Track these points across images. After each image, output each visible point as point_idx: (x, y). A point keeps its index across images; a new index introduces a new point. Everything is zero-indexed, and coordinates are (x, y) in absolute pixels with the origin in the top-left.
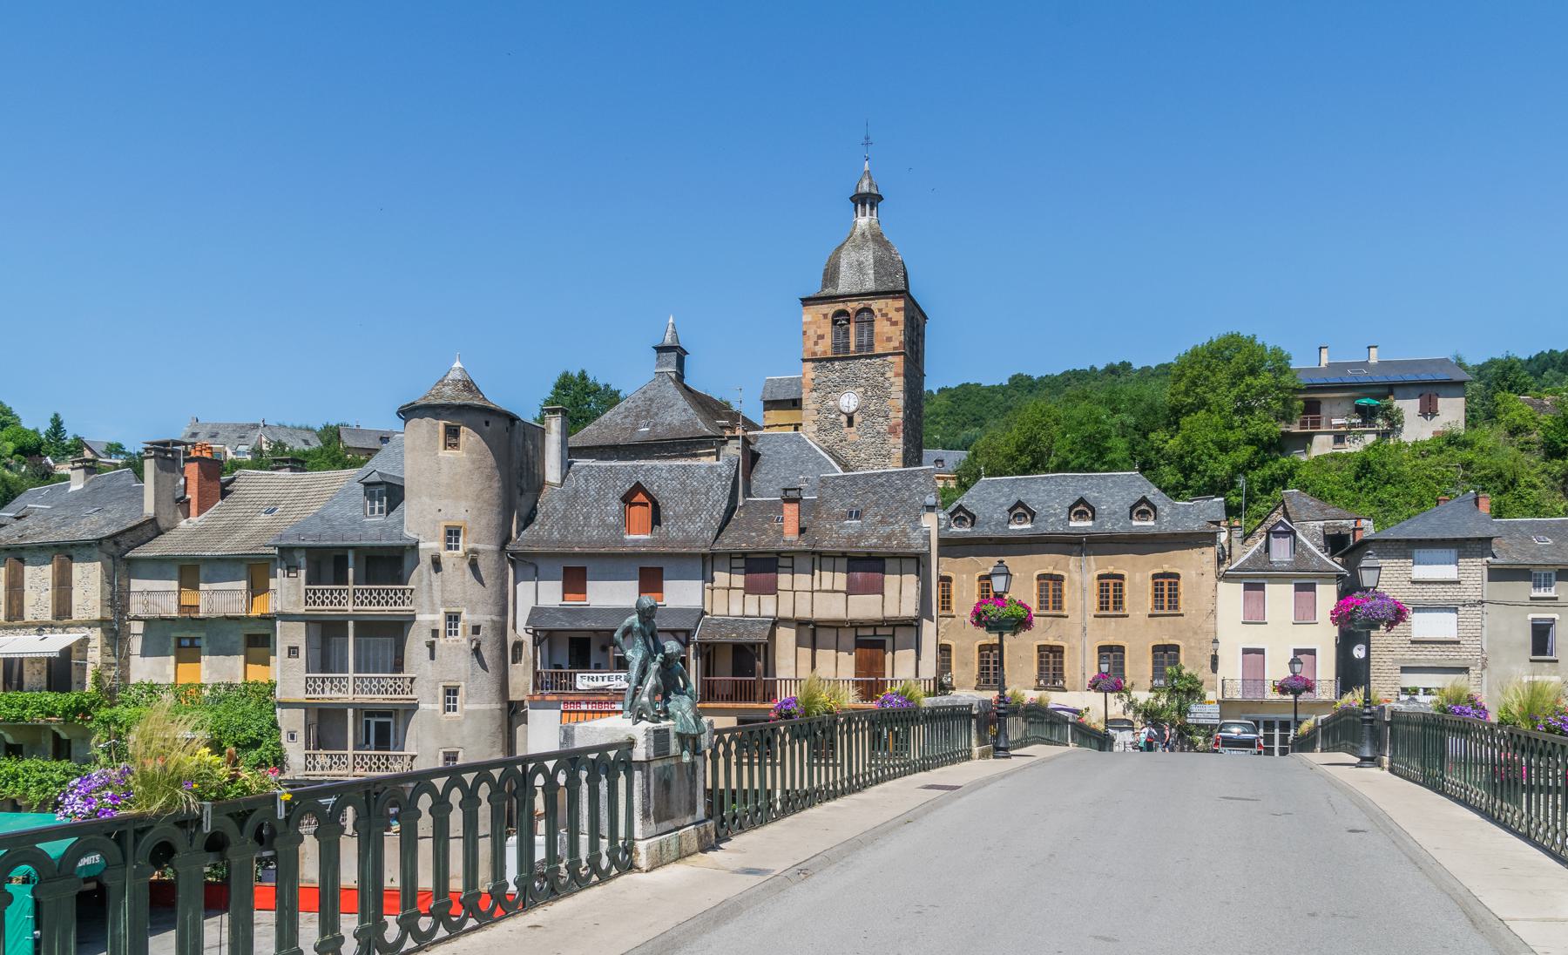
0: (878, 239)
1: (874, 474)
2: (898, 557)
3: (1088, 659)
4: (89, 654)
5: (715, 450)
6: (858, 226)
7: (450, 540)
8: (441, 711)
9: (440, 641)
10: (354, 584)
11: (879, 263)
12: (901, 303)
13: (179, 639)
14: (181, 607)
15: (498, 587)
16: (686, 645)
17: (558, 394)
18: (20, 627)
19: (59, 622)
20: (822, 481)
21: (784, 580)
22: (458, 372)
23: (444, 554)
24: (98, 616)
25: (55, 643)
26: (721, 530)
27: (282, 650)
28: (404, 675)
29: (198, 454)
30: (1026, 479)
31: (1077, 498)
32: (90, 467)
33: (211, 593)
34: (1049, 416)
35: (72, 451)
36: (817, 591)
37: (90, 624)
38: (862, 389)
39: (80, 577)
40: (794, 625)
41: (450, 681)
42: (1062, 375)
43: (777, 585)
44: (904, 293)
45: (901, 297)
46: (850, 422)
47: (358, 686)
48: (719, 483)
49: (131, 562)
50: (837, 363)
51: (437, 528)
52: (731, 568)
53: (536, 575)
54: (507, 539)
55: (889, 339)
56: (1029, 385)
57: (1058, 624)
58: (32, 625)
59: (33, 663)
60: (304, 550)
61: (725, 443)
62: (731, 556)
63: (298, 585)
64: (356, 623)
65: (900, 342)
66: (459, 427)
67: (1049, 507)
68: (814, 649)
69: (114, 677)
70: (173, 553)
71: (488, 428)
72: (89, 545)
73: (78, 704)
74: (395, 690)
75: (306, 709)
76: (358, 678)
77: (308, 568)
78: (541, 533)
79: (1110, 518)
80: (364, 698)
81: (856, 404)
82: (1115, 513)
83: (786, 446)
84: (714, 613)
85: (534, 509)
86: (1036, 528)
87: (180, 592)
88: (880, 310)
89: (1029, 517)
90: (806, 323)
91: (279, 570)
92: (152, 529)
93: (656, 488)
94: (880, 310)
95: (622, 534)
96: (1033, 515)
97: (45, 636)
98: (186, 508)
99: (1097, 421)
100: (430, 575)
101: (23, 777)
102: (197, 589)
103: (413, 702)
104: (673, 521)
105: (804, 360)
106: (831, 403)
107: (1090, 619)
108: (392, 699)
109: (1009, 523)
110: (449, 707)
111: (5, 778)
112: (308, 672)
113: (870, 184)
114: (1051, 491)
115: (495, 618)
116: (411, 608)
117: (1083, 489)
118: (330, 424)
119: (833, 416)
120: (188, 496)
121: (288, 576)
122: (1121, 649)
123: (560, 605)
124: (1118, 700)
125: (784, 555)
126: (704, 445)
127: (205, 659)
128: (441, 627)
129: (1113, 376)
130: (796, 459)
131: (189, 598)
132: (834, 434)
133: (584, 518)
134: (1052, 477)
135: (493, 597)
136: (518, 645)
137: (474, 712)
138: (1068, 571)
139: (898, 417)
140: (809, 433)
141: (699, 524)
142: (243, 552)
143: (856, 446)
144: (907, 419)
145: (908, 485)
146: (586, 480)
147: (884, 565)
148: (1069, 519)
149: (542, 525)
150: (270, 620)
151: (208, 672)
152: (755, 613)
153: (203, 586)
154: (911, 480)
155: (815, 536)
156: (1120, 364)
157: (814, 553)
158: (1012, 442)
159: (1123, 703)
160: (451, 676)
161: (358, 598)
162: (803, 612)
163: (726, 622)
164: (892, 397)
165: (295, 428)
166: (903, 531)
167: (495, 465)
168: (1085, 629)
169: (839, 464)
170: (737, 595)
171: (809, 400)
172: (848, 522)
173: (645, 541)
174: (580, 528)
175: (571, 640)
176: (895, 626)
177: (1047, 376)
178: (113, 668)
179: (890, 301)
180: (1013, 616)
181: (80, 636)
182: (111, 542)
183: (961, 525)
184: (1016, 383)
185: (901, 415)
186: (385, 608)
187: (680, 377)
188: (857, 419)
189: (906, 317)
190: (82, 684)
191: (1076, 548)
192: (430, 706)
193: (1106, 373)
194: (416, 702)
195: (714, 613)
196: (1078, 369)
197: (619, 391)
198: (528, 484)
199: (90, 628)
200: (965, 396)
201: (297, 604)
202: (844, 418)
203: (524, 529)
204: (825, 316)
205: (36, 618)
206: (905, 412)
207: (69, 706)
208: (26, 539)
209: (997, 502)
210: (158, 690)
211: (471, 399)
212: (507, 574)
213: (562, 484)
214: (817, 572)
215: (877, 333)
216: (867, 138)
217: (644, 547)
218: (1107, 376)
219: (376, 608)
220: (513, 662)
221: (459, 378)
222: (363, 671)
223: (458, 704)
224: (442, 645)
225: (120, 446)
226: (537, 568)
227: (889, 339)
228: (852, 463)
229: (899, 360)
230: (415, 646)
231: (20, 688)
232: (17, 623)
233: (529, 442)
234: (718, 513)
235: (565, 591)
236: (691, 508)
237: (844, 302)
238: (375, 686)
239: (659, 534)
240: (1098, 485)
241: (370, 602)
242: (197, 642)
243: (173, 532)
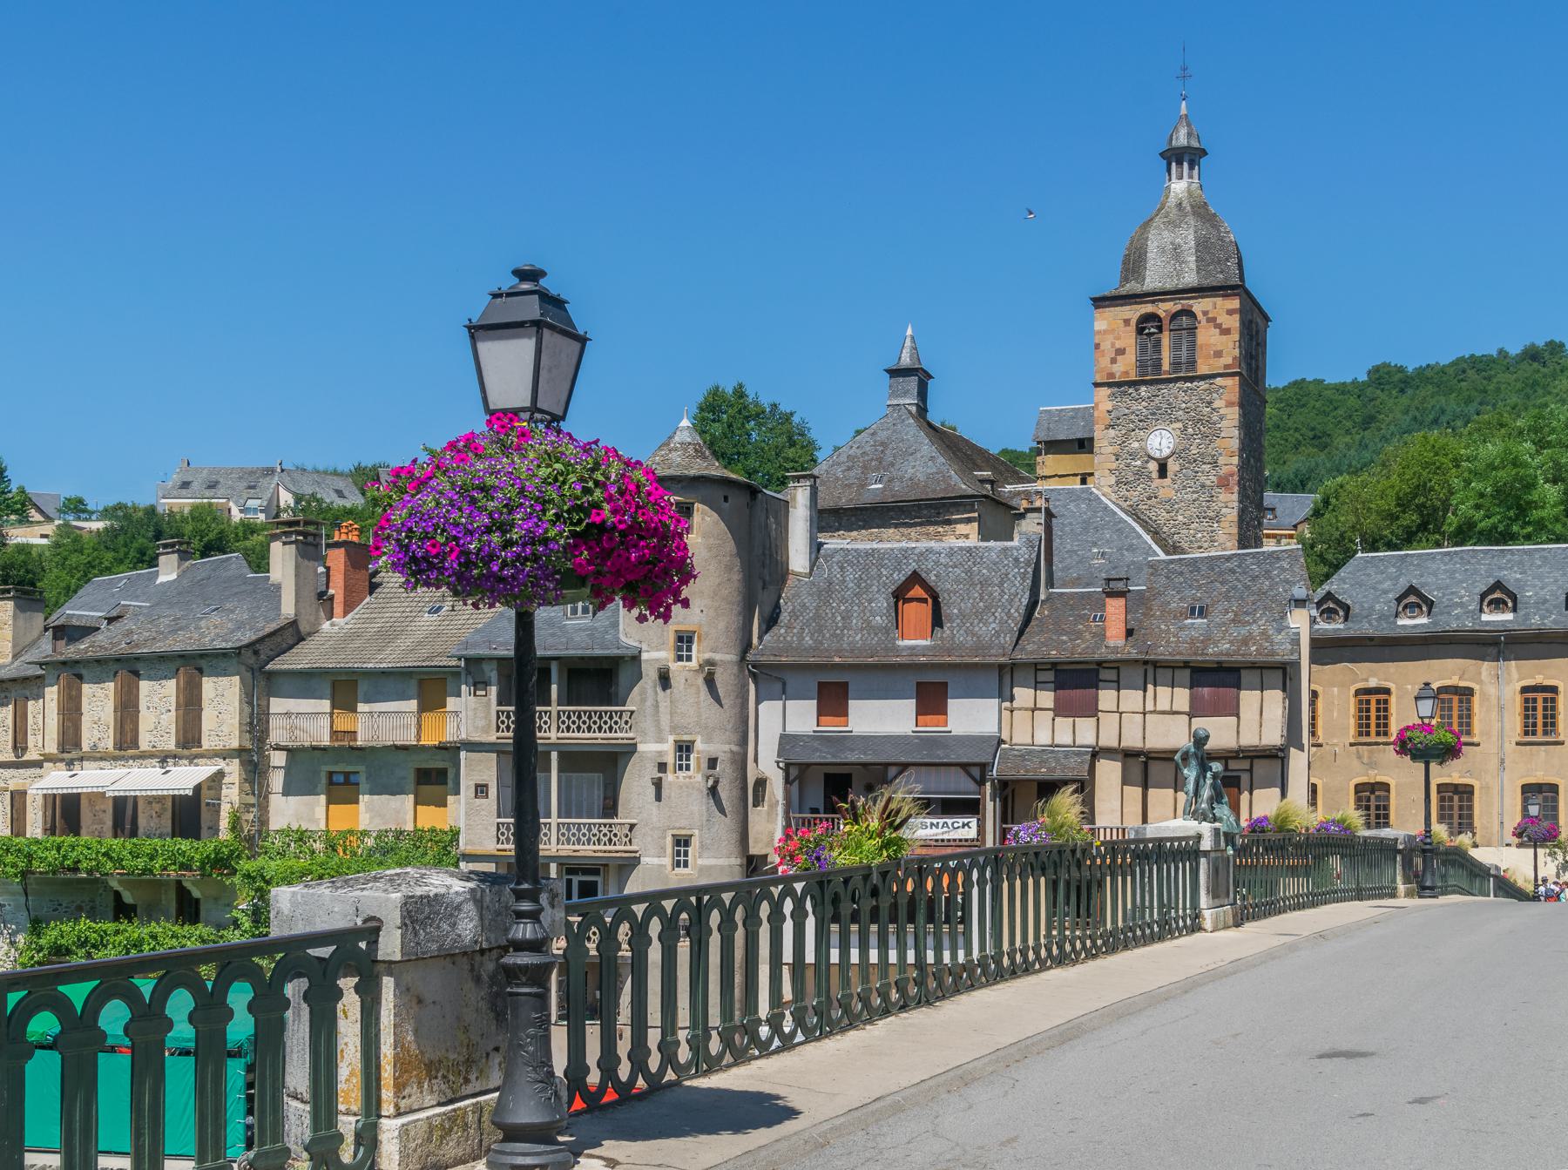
0: (1201, 211)
1: (1219, 557)
2: (1258, 668)
3: (1507, 800)
4: (224, 791)
5: (976, 515)
6: (1172, 194)
7: (680, 649)
8: (669, 867)
9: (669, 777)
10: (558, 705)
11: (1202, 246)
12: (1235, 303)
13: (331, 774)
14: (334, 734)
15: (737, 710)
16: (981, 782)
17: (703, 419)
18: (134, 758)
19: (186, 752)
20: (1152, 567)
21: (1106, 698)
22: (686, 433)
23: (675, 667)
24: (235, 744)
25: (184, 778)
26: (1021, 632)
27: (468, 787)
28: (619, 821)
29: (344, 537)
30: (1420, 555)
31: (1491, 581)
32: (185, 552)
33: (376, 716)
34: (1447, 455)
35: (18, 510)
36: (1151, 712)
37: (225, 755)
38: (1180, 425)
39: (212, 695)
40: (1120, 756)
41: (680, 828)
42: (1453, 364)
43: (1097, 704)
44: (1235, 289)
45: (1235, 295)
46: (1163, 471)
47: (563, 835)
48: (1016, 570)
49: (271, 675)
50: (1143, 388)
51: (665, 633)
52: (1036, 682)
53: (784, 693)
54: (747, 646)
55: (1218, 354)
56: (1401, 381)
58: (151, 756)
59: (150, 803)
60: (495, 662)
61: (1022, 516)
62: (1036, 667)
63: (488, 704)
64: (562, 755)
65: (1234, 359)
66: (693, 504)
67: (1452, 593)
68: (1145, 787)
69: (253, 821)
70: (326, 665)
71: (727, 505)
72: (225, 655)
73: (217, 854)
74: (610, 840)
75: (497, 863)
76: (564, 824)
77: (499, 683)
78: (789, 638)
79: (1539, 609)
80: (566, 850)
82: (1545, 601)
83: (1072, 506)
84: (1014, 742)
85: (777, 606)
86: (1435, 624)
87: (331, 714)
88: (1205, 313)
89: (1424, 609)
90: (1099, 332)
91: (463, 687)
92: (292, 634)
93: (933, 578)
94: (1205, 313)
95: (894, 639)
96: (1430, 604)
97: (168, 769)
98: (329, 607)
99: (1516, 463)
100: (656, 693)
101: (149, 944)
102: (354, 710)
103: (633, 855)
104: (959, 621)
105: (1097, 385)
106: (1136, 445)
107: (1510, 747)
108: (605, 852)
109: (1396, 616)
110: (679, 862)
111: (125, 946)
112: (499, 817)
113: (1189, 135)
114: (1455, 571)
115: (735, 748)
116: (631, 735)
117: (1501, 568)
118: (363, 465)
119: (1139, 463)
120: (331, 591)
121: (475, 695)
122: (1554, 788)
123: (814, 732)
124: (1549, 859)
125: (1107, 665)
126: (961, 509)
127: (364, 799)
128: (670, 759)
129: (1535, 365)
130: (1086, 525)
131: (344, 722)
132: (1139, 489)
133: (843, 618)
134: (1456, 552)
135: (733, 721)
136: (761, 783)
137: (710, 867)
138: (1480, 682)
139: (1230, 463)
140: (1102, 486)
141: (993, 625)
142: (415, 664)
144: (1243, 467)
145: (1267, 572)
146: (842, 568)
147: (1240, 678)
148: (1481, 610)
149: (789, 627)
150: (450, 751)
151: (368, 816)
152: (1069, 741)
153: (361, 707)
154: (1271, 564)
155: (1148, 640)
156: (1547, 344)
157: (1146, 662)
158: (1391, 493)
159: (1556, 862)
160: (683, 823)
161: (563, 722)
162: (1132, 740)
163: (1030, 752)
164: (1222, 435)
165: (318, 472)
166: (1264, 633)
167: (735, 551)
168: (1502, 762)
169: (1148, 531)
170: (1044, 718)
171: (1105, 441)
172: (1189, 621)
173: (926, 647)
174: (838, 632)
175: (828, 777)
176: (1252, 758)
177: (1428, 366)
178: (251, 809)
179: (1219, 301)
180: (1441, 743)
181: (214, 769)
182: (250, 653)
183: (1329, 619)
185: (1235, 460)
186: (597, 735)
187: (922, 410)
188: (1173, 466)
189: (1242, 322)
190: (215, 830)
191: (1492, 650)
192: (656, 861)
193: (1524, 359)
194: (637, 855)
195: (1014, 742)
196: (1478, 354)
197: (792, 414)
198: (770, 575)
199: (224, 759)
200: (1299, 400)
201: (486, 730)
203: (766, 632)
204: (1127, 322)
205: (154, 747)
206: (1240, 456)
207: (208, 857)
208: (137, 646)
209: (1378, 586)
210: (310, 837)
211: (706, 468)
212: (748, 690)
213: (811, 574)
214: (1150, 687)
215: (1201, 346)
217: (924, 656)
218: (1524, 365)
219: (587, 735)
220: (755, 805)
221: (689, 440)
222: (574, 815)
223: (690, 858)
224: (670, 783)
225: (81, 501)
226: (784, 684)
227: (1218, 354)
229: (1232, 383)
230: (635, 786)
231: (134, 833)
232: (131, 752)
233: (772, 520)
234: (1017, 611)
235: (821, 712)
236: (981, 604)
237: (1153, 302)
238: (584, 835)
239: (942, 638)
240: (1521, 563)
241: (579, 728)
242: (352, 778)
243: (316, 637)
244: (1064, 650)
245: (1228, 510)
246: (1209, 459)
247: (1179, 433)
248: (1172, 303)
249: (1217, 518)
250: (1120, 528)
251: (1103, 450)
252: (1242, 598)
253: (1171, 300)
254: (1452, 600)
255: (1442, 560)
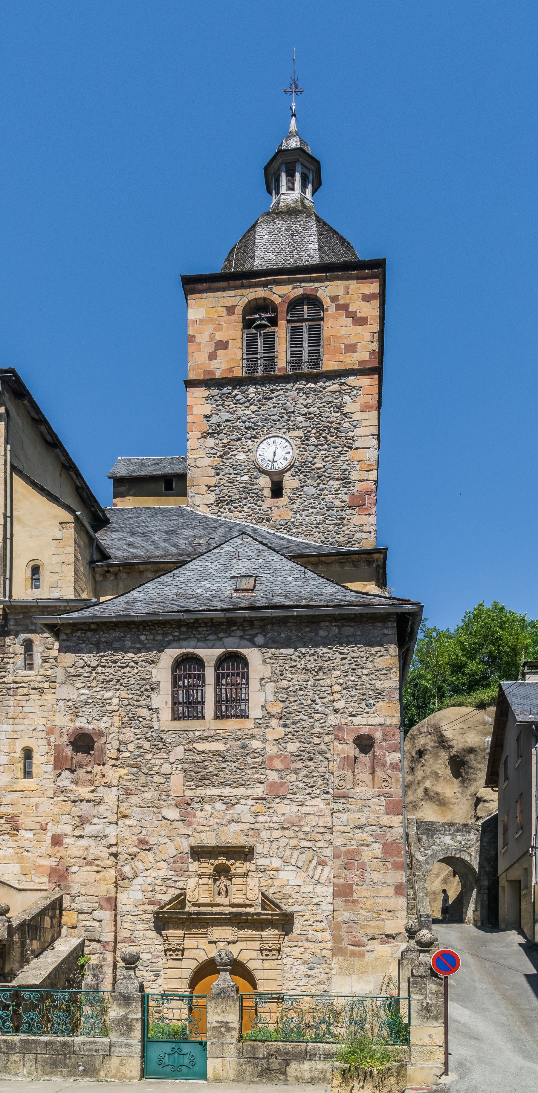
38: (300, 433)
46: (277, 491)
50: (252, 390)
55: (351, 348)
81: (289, 457)
94: (334, 299)
106: (242, 456)
132: (246, 509)
164: (356, 444)
179: (353, 284)
188: (290, 483)
202: (264, 482)
204: (230, 310)
215: (328, 339)
227: (351, 348)
237: (265, 285)
245: (364, 535)
246: (338, 474)
247: (299, 442)
248: (290, 287)
251: (198, 463)
253: (290, 282)
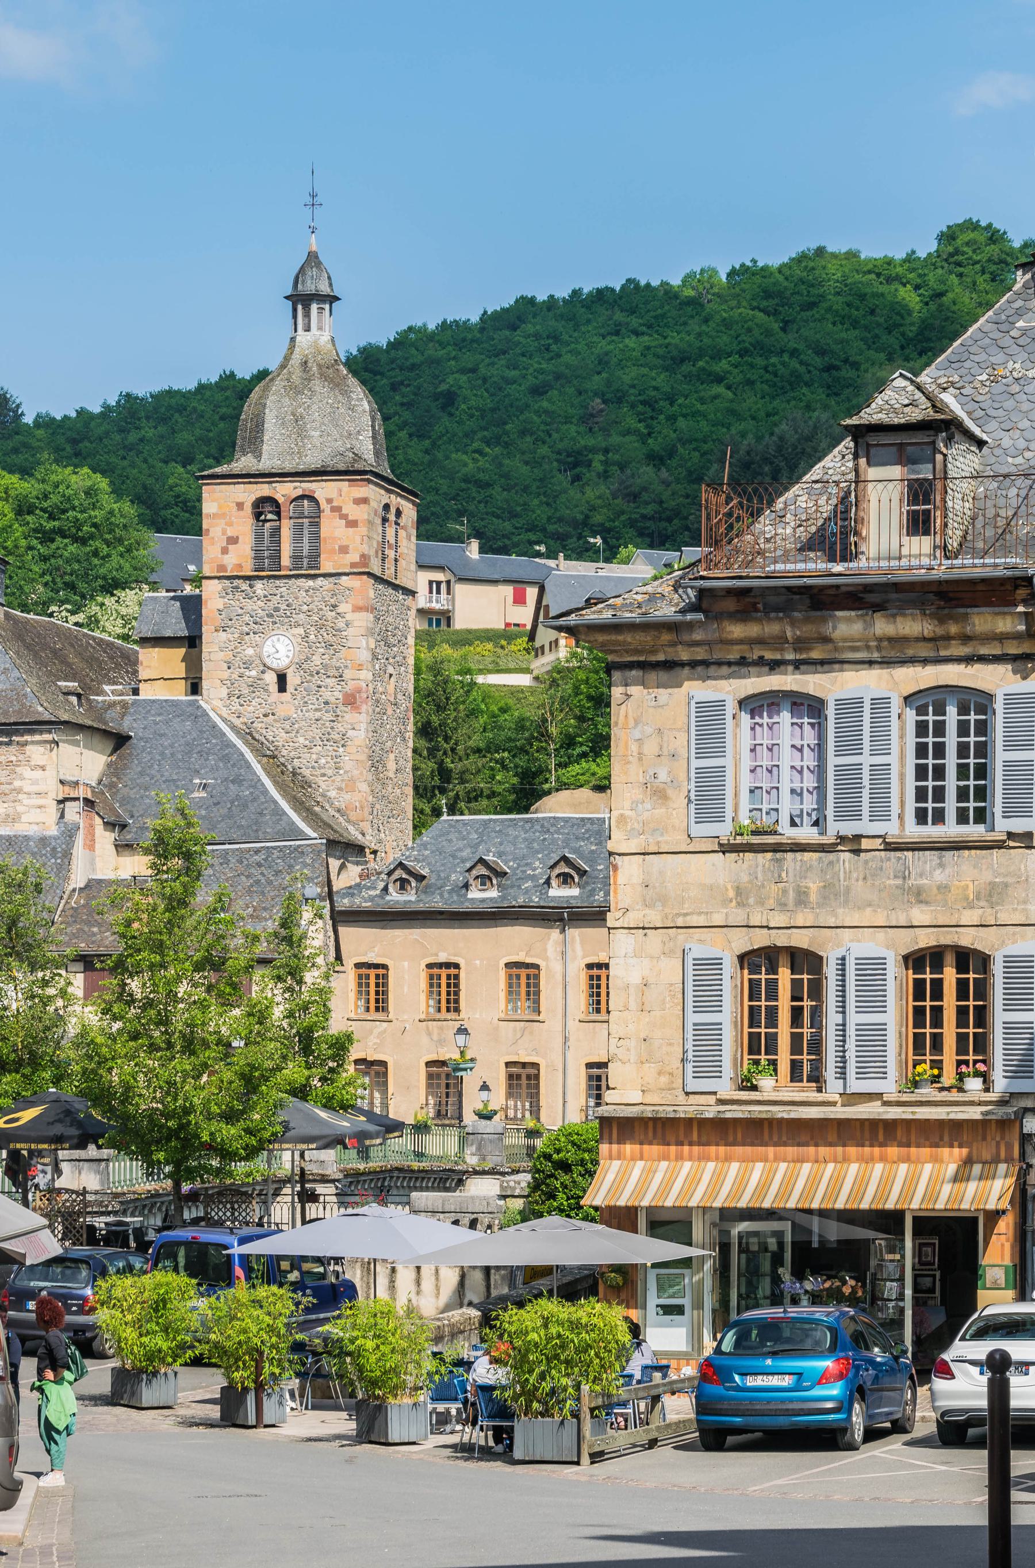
38: (300, 631)
46: (282, 687)
55: (344, 550)
57: (531, 1033)
81: (291, 654)
94: (329, 501)
119: (254, 673)
138: (546, 959)
143: (291, 725)
145: (291, 867)
184: (957, 252)
188: (292, 681)
202: (271, 678)
204: (240, 506)
209: (459, 854)
216: (313, 196)
227: (344, 550)
228: (284, 752)
244: (93, 942)
249: (344, 741)
250: (227, 753)
251: (213, 657)
252: (263, 893)
254: (525, 871)
255: (523, 827)
